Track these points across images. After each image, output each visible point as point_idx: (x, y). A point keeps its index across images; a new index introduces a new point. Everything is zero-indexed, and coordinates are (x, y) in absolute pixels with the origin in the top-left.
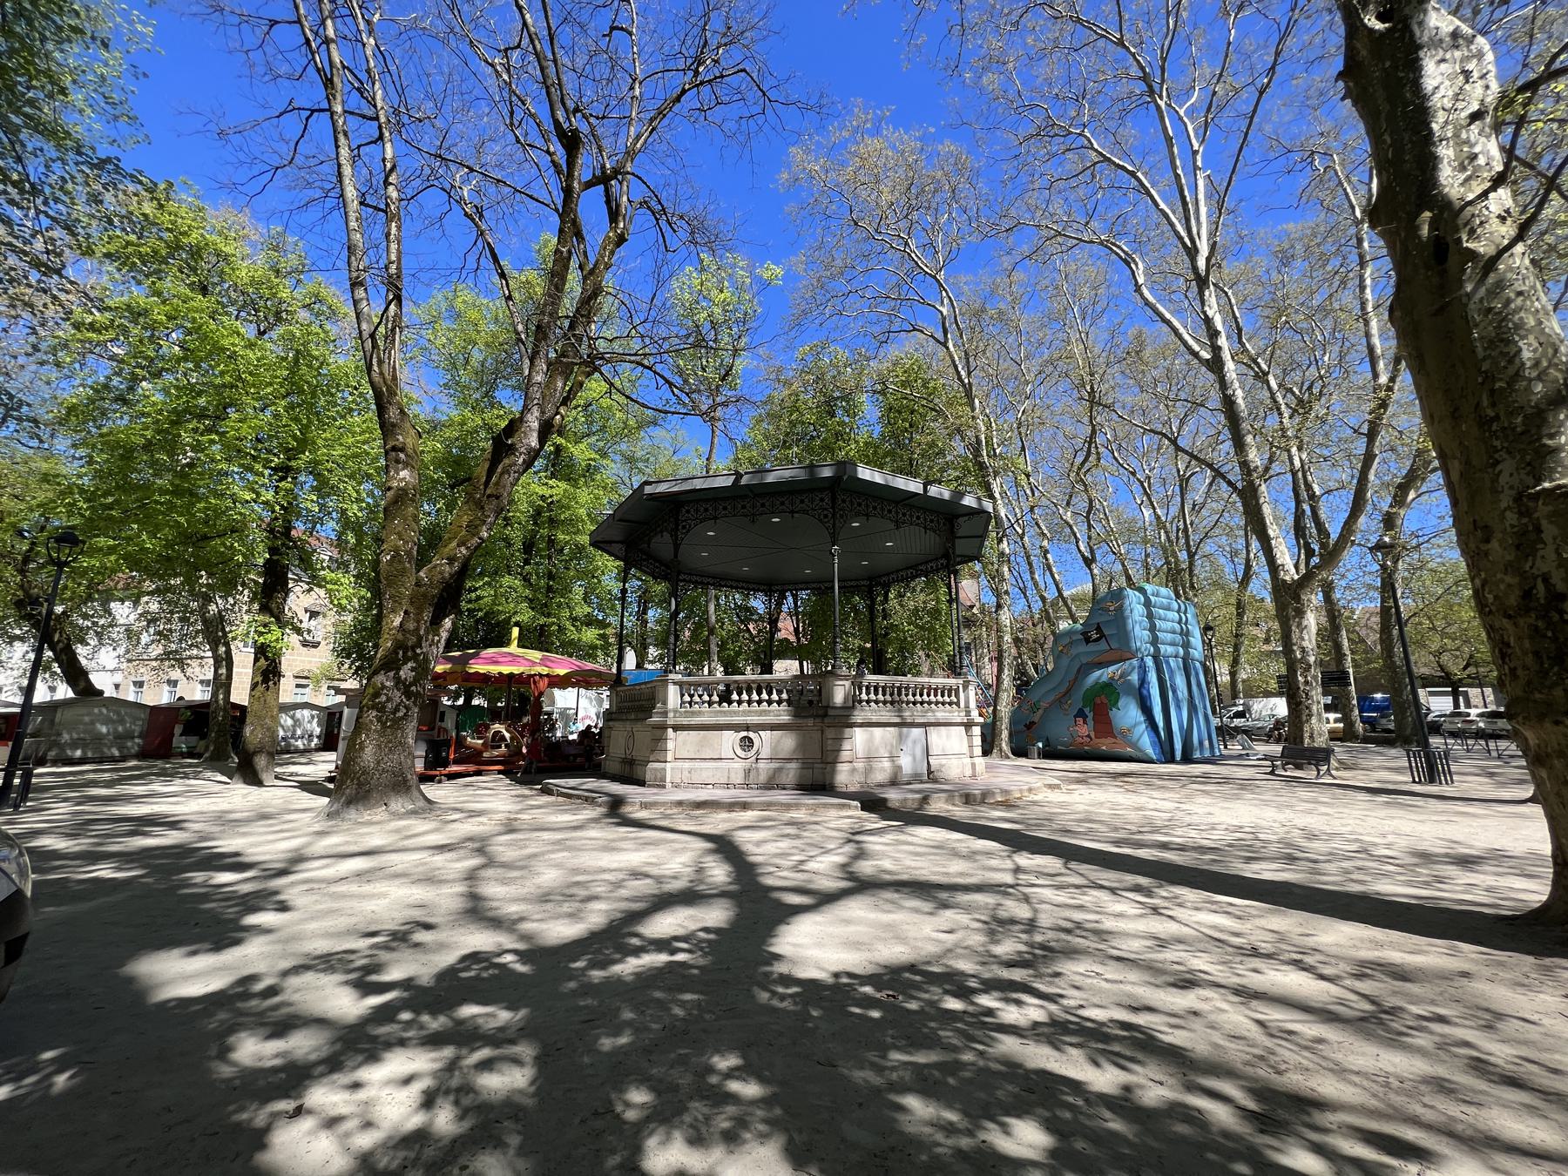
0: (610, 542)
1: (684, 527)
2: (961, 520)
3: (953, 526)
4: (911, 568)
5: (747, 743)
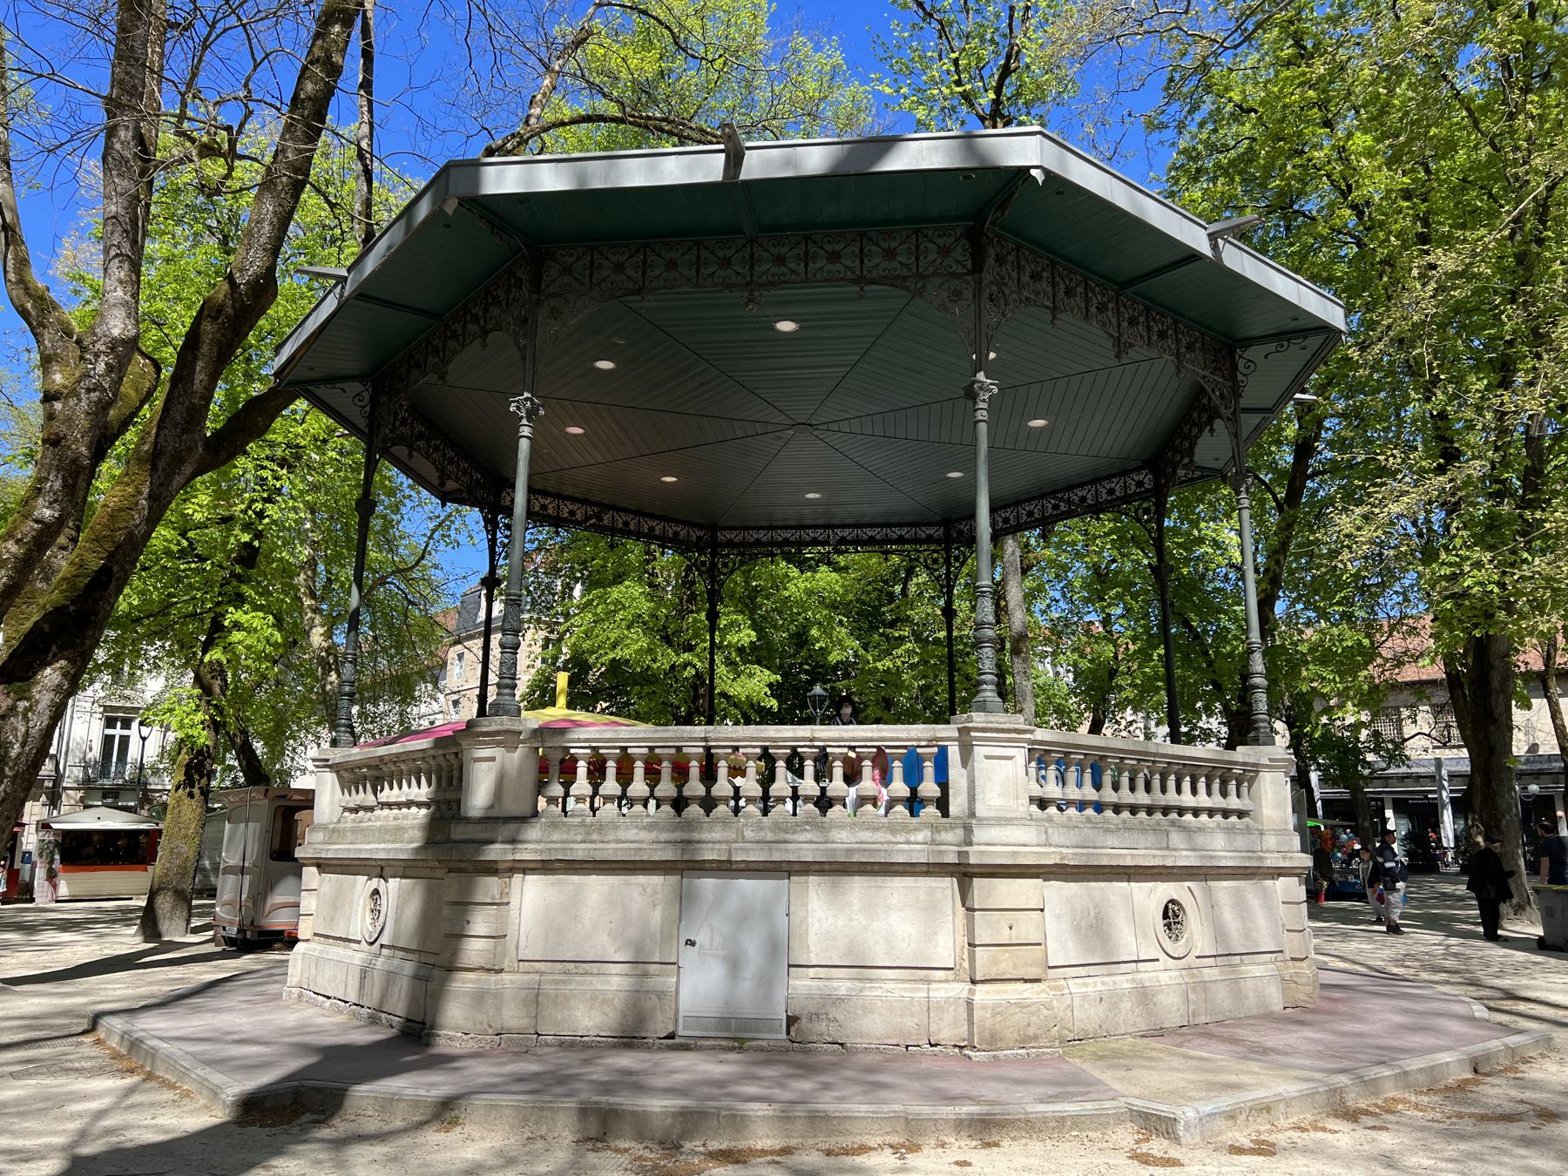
0: (331, 380)
2: (1256, 352)
3: (1234, 366)
4: (1053, 494)
5: (1172, 915)
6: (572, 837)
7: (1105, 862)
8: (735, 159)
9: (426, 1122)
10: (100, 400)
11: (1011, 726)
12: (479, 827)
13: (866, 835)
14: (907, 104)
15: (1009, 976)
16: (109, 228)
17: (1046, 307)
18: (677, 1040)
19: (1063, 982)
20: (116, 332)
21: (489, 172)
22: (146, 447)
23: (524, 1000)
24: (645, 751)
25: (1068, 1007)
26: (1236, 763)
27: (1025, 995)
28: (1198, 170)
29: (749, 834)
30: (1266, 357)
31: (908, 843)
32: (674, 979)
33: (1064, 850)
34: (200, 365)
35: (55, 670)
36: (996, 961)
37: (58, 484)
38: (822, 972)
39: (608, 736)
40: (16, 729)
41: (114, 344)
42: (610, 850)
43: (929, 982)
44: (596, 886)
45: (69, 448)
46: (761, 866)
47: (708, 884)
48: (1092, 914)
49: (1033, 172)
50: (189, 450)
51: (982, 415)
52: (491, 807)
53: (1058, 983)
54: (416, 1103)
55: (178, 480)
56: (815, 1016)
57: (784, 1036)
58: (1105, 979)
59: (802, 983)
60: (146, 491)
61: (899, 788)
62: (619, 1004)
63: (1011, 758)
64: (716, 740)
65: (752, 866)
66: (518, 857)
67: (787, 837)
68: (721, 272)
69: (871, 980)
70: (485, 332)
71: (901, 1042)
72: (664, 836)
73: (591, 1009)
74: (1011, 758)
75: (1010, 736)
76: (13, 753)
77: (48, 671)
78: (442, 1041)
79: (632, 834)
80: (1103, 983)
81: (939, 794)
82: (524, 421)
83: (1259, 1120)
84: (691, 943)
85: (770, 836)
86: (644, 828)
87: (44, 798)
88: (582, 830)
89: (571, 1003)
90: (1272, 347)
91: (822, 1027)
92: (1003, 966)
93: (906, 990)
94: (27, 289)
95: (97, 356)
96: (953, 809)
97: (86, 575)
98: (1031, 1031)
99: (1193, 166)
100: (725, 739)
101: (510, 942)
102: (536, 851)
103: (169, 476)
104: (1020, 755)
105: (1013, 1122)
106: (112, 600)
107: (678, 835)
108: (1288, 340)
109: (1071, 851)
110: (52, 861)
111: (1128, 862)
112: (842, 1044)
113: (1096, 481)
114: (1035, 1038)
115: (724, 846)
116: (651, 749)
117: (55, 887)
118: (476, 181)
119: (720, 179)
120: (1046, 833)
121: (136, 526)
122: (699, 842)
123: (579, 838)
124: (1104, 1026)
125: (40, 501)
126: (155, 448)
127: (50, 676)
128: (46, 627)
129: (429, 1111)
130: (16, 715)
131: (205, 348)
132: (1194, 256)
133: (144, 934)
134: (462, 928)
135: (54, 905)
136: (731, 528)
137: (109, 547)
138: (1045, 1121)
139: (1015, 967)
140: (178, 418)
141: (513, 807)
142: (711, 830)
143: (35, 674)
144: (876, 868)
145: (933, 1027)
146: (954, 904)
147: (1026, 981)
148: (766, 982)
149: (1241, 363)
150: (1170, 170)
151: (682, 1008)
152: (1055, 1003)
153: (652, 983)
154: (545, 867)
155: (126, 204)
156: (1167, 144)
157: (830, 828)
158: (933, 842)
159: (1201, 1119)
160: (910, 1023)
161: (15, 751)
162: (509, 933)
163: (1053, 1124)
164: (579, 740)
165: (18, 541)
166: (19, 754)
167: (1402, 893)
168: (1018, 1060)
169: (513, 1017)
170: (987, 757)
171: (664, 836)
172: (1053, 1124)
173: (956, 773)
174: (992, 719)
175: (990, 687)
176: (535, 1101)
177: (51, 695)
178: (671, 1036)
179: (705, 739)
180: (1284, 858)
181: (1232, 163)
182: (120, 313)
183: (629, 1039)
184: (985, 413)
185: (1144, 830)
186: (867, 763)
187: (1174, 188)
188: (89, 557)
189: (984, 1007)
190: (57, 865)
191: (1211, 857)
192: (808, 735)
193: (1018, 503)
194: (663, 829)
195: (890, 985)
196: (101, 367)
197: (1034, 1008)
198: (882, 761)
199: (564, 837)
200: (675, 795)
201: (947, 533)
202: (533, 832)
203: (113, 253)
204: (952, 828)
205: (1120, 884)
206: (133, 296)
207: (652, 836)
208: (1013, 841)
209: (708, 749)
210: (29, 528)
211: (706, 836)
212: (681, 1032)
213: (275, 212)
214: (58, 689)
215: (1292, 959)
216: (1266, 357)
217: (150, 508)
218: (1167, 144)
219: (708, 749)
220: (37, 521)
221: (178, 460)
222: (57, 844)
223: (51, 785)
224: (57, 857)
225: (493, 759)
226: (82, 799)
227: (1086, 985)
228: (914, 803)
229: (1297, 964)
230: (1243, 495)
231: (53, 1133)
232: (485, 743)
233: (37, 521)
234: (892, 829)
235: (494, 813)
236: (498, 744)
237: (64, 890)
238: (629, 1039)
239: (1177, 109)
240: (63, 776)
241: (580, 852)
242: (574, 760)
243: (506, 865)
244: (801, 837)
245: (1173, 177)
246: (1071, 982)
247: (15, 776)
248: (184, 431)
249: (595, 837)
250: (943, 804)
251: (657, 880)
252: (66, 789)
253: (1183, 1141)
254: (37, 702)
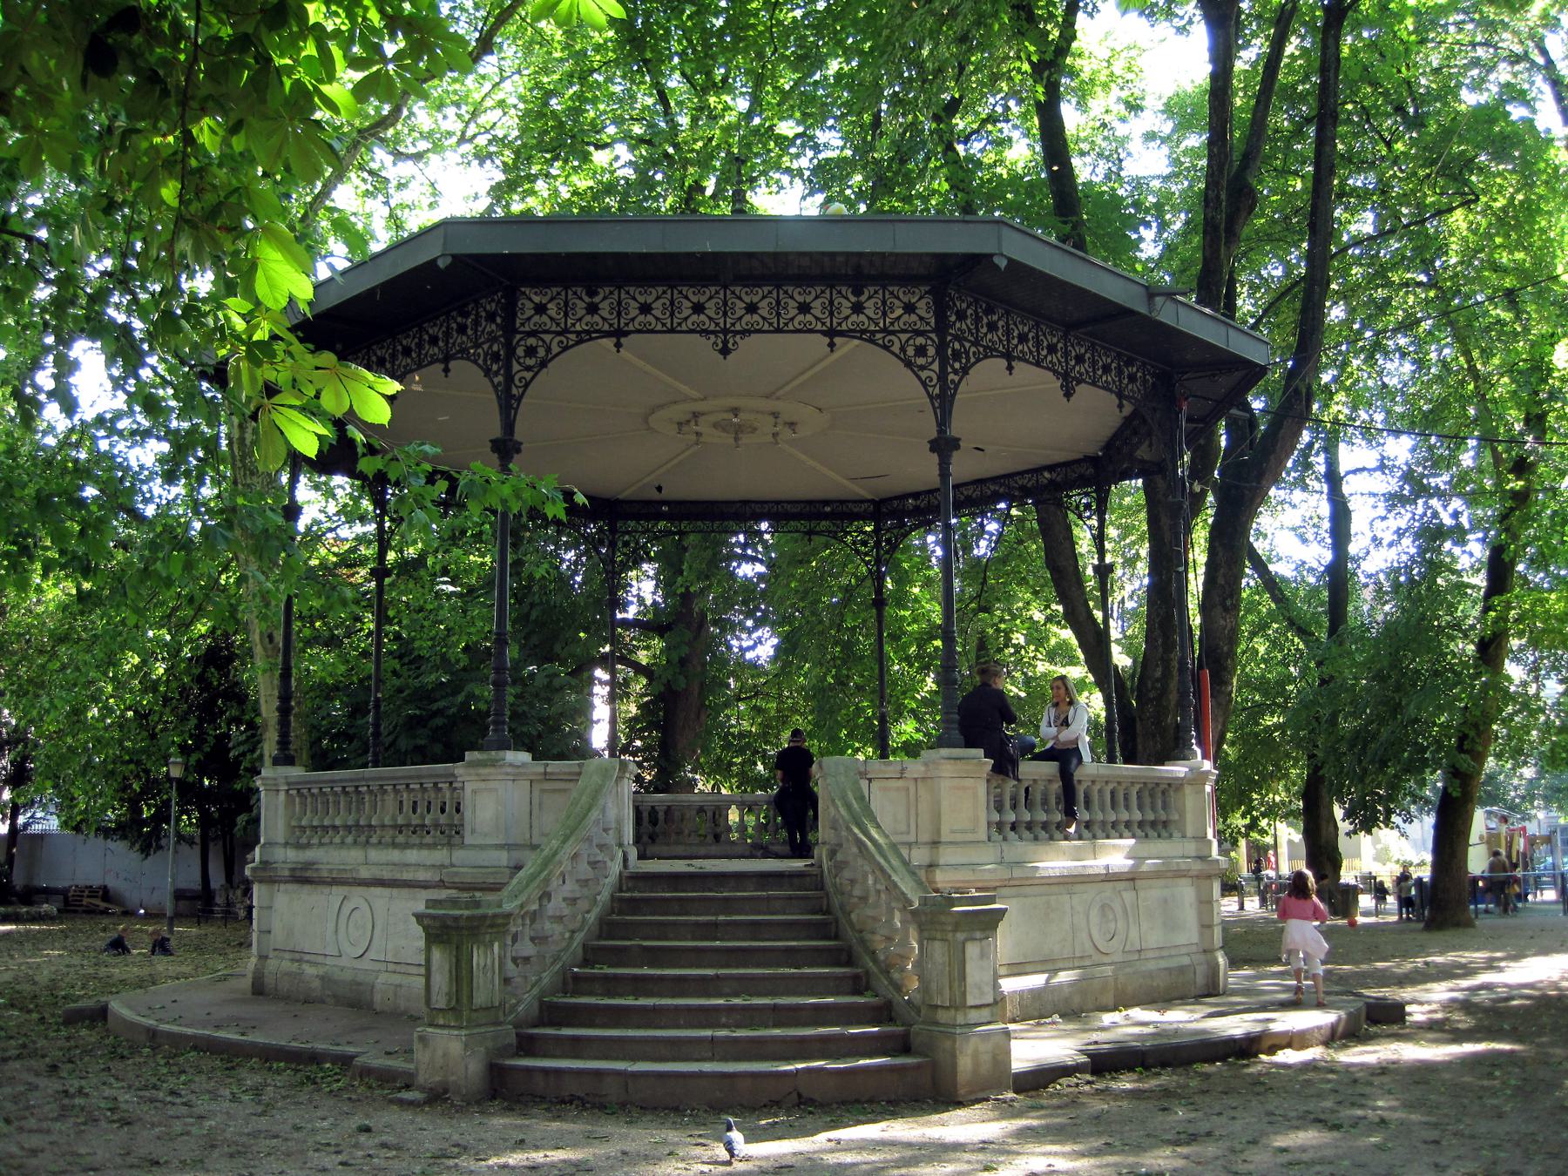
1: (531, 352)
70: (447, 359)
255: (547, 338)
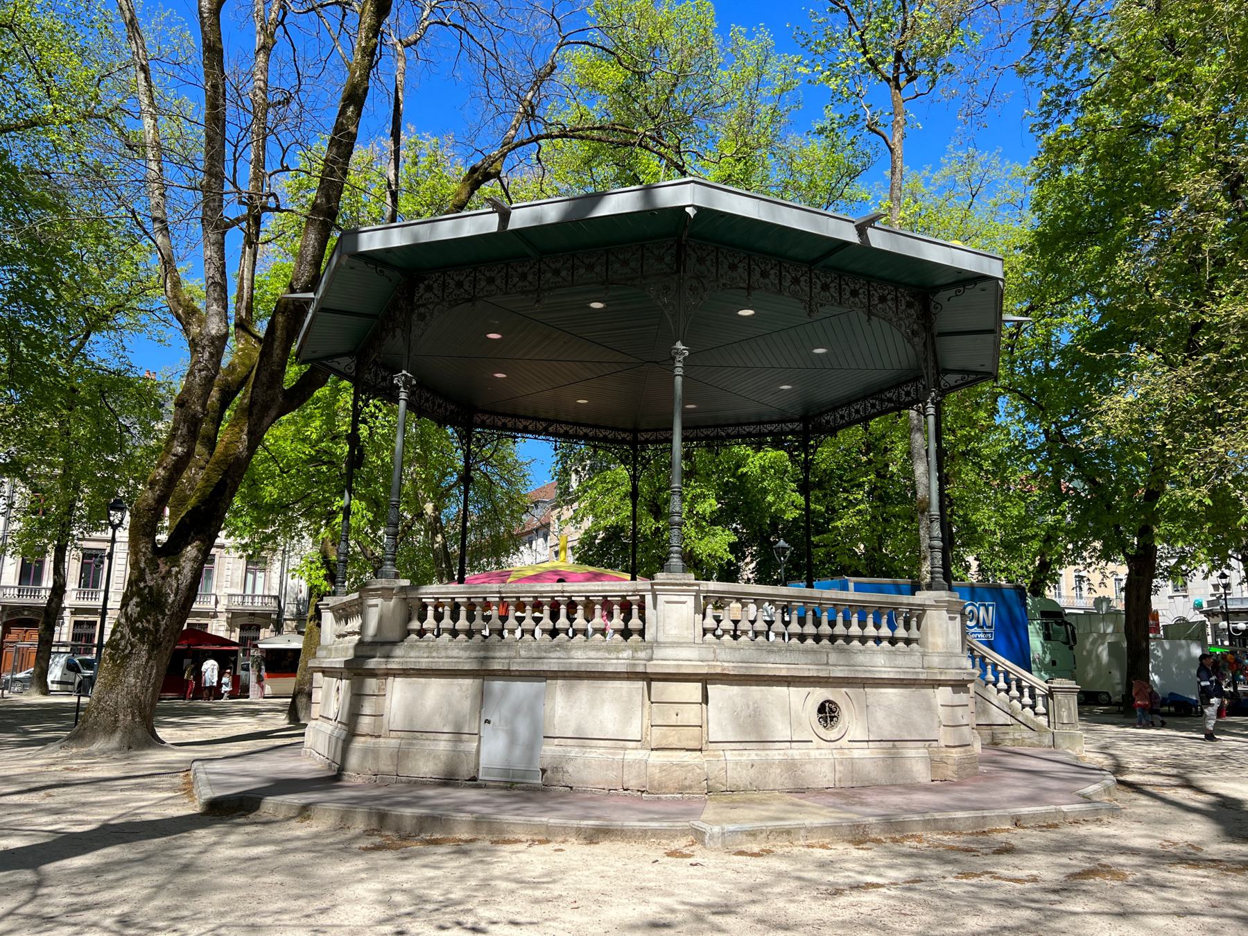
2: (942, 296)
5: (827, 712)
6: (421, 655)
7: (762, 673)
8: (505, 216)
9: (293, 818)
10: (207, 376)
11: (682, 582)
12: (368, 648)
13: (593, 654)
14: (821, 77)
15: (674, 746)
16: (207, 266)
17: (741, 288)
18: (478, 782)
19: (722, 753)
20: (213, 332)
21: (363, 237)
22: (246, 401)
23: (391, 755)
24: (465, 600)
25: (722, 769)
26: (901, 604)
27: (685, 759)
28: (1067, 103)
29: (523, 653)
30: (949, 300)
31: (618, 658)
32: (476, 744)
33: (726, 664)
34: (277, 343)
35: (193, 548)
36: (665, 736)
37: (185, 431)
38: (563, 741)
39: (443, 590)
40: (171, 585)
41: (213, 340)
42: (443, 664)
43: (625, 749)
44: (436, 686)
45: (190, 407)
46: (528, 674)
47: (497, 685)
48: (751, 708)
49: (688, 210)
50: (273, 400)
51: (679, 371)
52: (375, 635)
53: (717, 753)
54: (290, 806)
55: (267, 420)
56: (556, 769)
57: (540, 782)
58: (759, 752)
59: (549, 750)
60: (246, 429)
61: (617, 622)
62: (443, 758)
63: (684, 603)
64: (506, 593)
65: (523, 673)
66: (389, 666)
67: (544, 654)
68: (521, 284)
69: (591, 747)
71: (606, 787)
72: (474, 654)
73: (428, 761)
74: (684, 603)
75: (681, 588)
76: (170, 601)
77: (189, 548)
78: (346, 778)
79: (455, 653)
80: (757, 755)
81: (623, 627)
82: (402, 389)
83: (779, 839)
84: (487, 721)
85: (535, 654)
86: (463, 649)
87: (271, 626)
88: (427, 650)
89: (417, 757)
90: (952, 292)
91: (559, 776)
92: (671, 740)
93: (611, 754)
94: (178, 301)
95: (203, 348)
96: (647, 636)
97: (211, 486)
98: (687, 783)
99: (1064, 100)
100: (511, 592)
101: (385, 719)
102: (399, 663)
103: (261, 419)
104: (691, 601)
105: (613, 831)
106: (228, 501)
107: (482, 654)
108: (964, 287)
109: (732, 664)
110: (260, 671)
111: (784, 673)
112: (571, 788)
113: (898, 385)
114: (690, 787)
115: (507, 661)
116: (469, 598)
117: (263, 688)
118: (356, 243)
119: (496, 229)
120: (714, 652)
121: (241, 453)
122: (494, 658)
123: (426, 655)
124: (755, 784)
125: (175, 443)
126: (251, 401)
127: (191, 551)
128: (187, 520)
129: (297, 812)
130: (171, 577)
131: (279, 333)
132: (846, 244)
133: (290, 719)
134: (359, 710)
135: (262, 700)
136: (647, 431)
137: (224, 467)
138: (633, 831)
139: (679, 740)
140: (264, 379)
141: (393, 634)
142: (501, 651)
143: (182, 550)
144: (597, 675)
145: (625, 778)
146: (643, 699)
147: (687, 750)
148: (532, 747)
149: (933, 304)
150: (1042, 106)
151: (482, 762)
152: (706, 765)
153: (462, 747)
154: (406, 673)
155: (216, 249)
156: (1035, 85)
157: (571, 649)
158: (633, 658)
159: (723, 834)
160: (611, 775)
161: (171, 599)
162: (385, 713)
163: (639, 834)
164: (426, 594)
165: (164, 468)
166: (174, 601)
167: (1216, 707)
168: (675, 800)
169: (385, 765)
170: (668, 602)
171: (474, 654)
172: (639, 834)
173: (649, 611)
174: (671, 576)
175: (676, 555)
176: (902, 900)
177: (192, 563)
178: (474, 779)
179: (499, 592)
180: (941, 673)
181: (1098, 94)
182: (216, 319)
183: (448, 780)
184: (680, 369)
185: (806, 651)
186: (598, 607)
187: (1048, 121)
188: (213, 474)
189: (653, 766)
190: (264, 673)
191: (869, 671)
192: (560, 589)
193: (835, 409)
194: (474, 650)
195: (602, 750)
196: (206, 355)
197: (690, 768)
198: (607, 605)
199: (417, 654)
200: (623, 627)
201: (806, 427)
202: (398, 651)
203: (210, 282)
204: (645, 649)
205: (779, 688)
206: (223, 308)
207: (466, 654)
208: (682, 658)
209: (501, 598)
210: (170, 459)
211: (498, 654)
212: (481, 777)
213: (316, 239)
214: (195, 559)
215: (946, 746)
216: (949, 300)
217: (249, 440)
218: (1035, 85)
219: (501, 598)
220: (174, 455)
221: (266, 408)
222: (262, 658)
223: (275, 617)
224: (263, 667)
225: (377, 606)
226: (296, 627)
227: (741, 755)
228: (626, 633)
229: (949, 750)
230: (930, 405)
231: (105, 814)
232: (373, 595)
233: (174, 455)
234: (609, 649)
235: (377, 639)
236: (379, 596)
237: (268, 690)
238: (448, 780)
239: (1041, 57)
240: (283, 611)
241: (424, 663)
242: (425, 606)
243: (381, 672)
244: (552, 655)
245: (1045, 112)
246: (728, 753)
247: (172, 615)
248: (268, 388)
249: (434, 654)
250: (642, 633)
251: (467, 682)
252: (285, 620)
253: (708, 846)
254: (183, 568)
255: (431, 307)
